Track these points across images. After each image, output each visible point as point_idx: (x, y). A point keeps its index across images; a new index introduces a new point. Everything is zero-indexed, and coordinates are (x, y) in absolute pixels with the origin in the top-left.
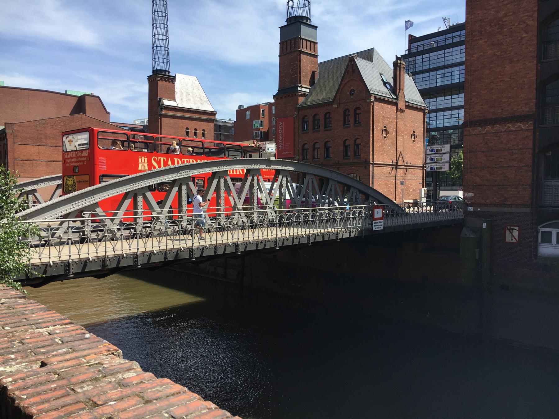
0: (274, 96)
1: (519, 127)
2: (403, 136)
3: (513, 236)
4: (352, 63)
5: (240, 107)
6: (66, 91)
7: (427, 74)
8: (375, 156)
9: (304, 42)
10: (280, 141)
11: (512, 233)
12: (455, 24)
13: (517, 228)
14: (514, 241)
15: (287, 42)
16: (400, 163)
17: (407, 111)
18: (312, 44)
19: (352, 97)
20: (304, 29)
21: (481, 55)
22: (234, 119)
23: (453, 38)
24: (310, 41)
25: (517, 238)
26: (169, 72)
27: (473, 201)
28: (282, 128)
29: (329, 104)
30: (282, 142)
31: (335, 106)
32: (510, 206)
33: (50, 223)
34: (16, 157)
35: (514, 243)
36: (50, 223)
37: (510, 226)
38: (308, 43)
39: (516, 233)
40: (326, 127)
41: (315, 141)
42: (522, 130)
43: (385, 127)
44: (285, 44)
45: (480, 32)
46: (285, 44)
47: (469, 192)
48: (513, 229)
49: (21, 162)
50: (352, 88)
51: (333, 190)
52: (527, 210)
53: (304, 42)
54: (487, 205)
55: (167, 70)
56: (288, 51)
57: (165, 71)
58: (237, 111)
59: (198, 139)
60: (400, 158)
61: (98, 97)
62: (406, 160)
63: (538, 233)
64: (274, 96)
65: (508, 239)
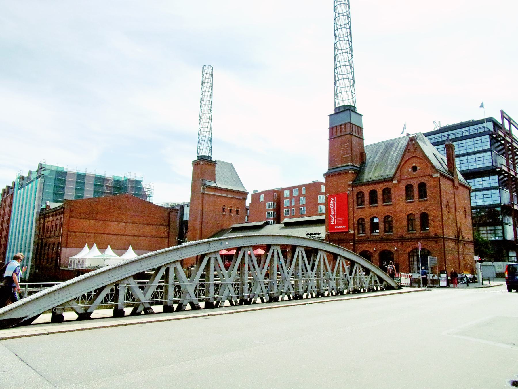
0: (324, 175)
4: (413, 142)
7: (466, 158)
9: (354, 126)
10: (331, 216)
12: (445, 126)
15: (336, 127)
17: (460, 188)
19: (415, 173)
23: (448, 135)
26: (211, 158)
28: (334, 203)
29: (390, 180)
30: (334, 217)
31: (395, 182)
33: (432, 285)
34: (70, 229)
36: (432, 285)
40: (420, 196)
41: (372, 216)
43: (448, 202)
44: (335, 129)
46: (335, 129)
49: (74, 234)
50: (414, 165)
51: (341, 265)
53: (354, 126)
55: (210, 156)
56: (338, 135)
57: (208, 157)
59: (370, 188)
64: (324, 175)
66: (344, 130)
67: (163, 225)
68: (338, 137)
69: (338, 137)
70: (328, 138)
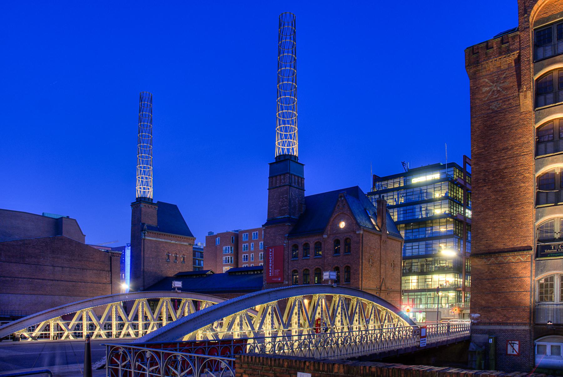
1: (519, 259)
2: (385, 265)
3: (513, 349)
5: (210, 233)
6: (43, 213)
8: (363, 282)
11: (513, 347)
13: (517, 342)
14: (515, 353)
16: (383, 288)
18: (300, 179)
20: (292, 164)
21: (485, 200)
22: (86, 243)
24: (298, 177)
25: (517, 351)
27: (479, 320)
32: (511, 324)
35: (514, 355)
37: (512, 341)
38: (296, 178)
39: (516, 347)
42: (521, 262)
45: (484, 180)
47: (475, 313)
48: (513, 343)
52: (527, 328)
54: (490, 324)
58: (206, 237)
60: (383, 284)
61: (75, 220)
62: (388, 285)
63: (534, 346)
65: (510, 351)
66: (283, 181)
67: (104, 271)
68: (277, 187)
69: (277, 187)
70: (305, 181)
